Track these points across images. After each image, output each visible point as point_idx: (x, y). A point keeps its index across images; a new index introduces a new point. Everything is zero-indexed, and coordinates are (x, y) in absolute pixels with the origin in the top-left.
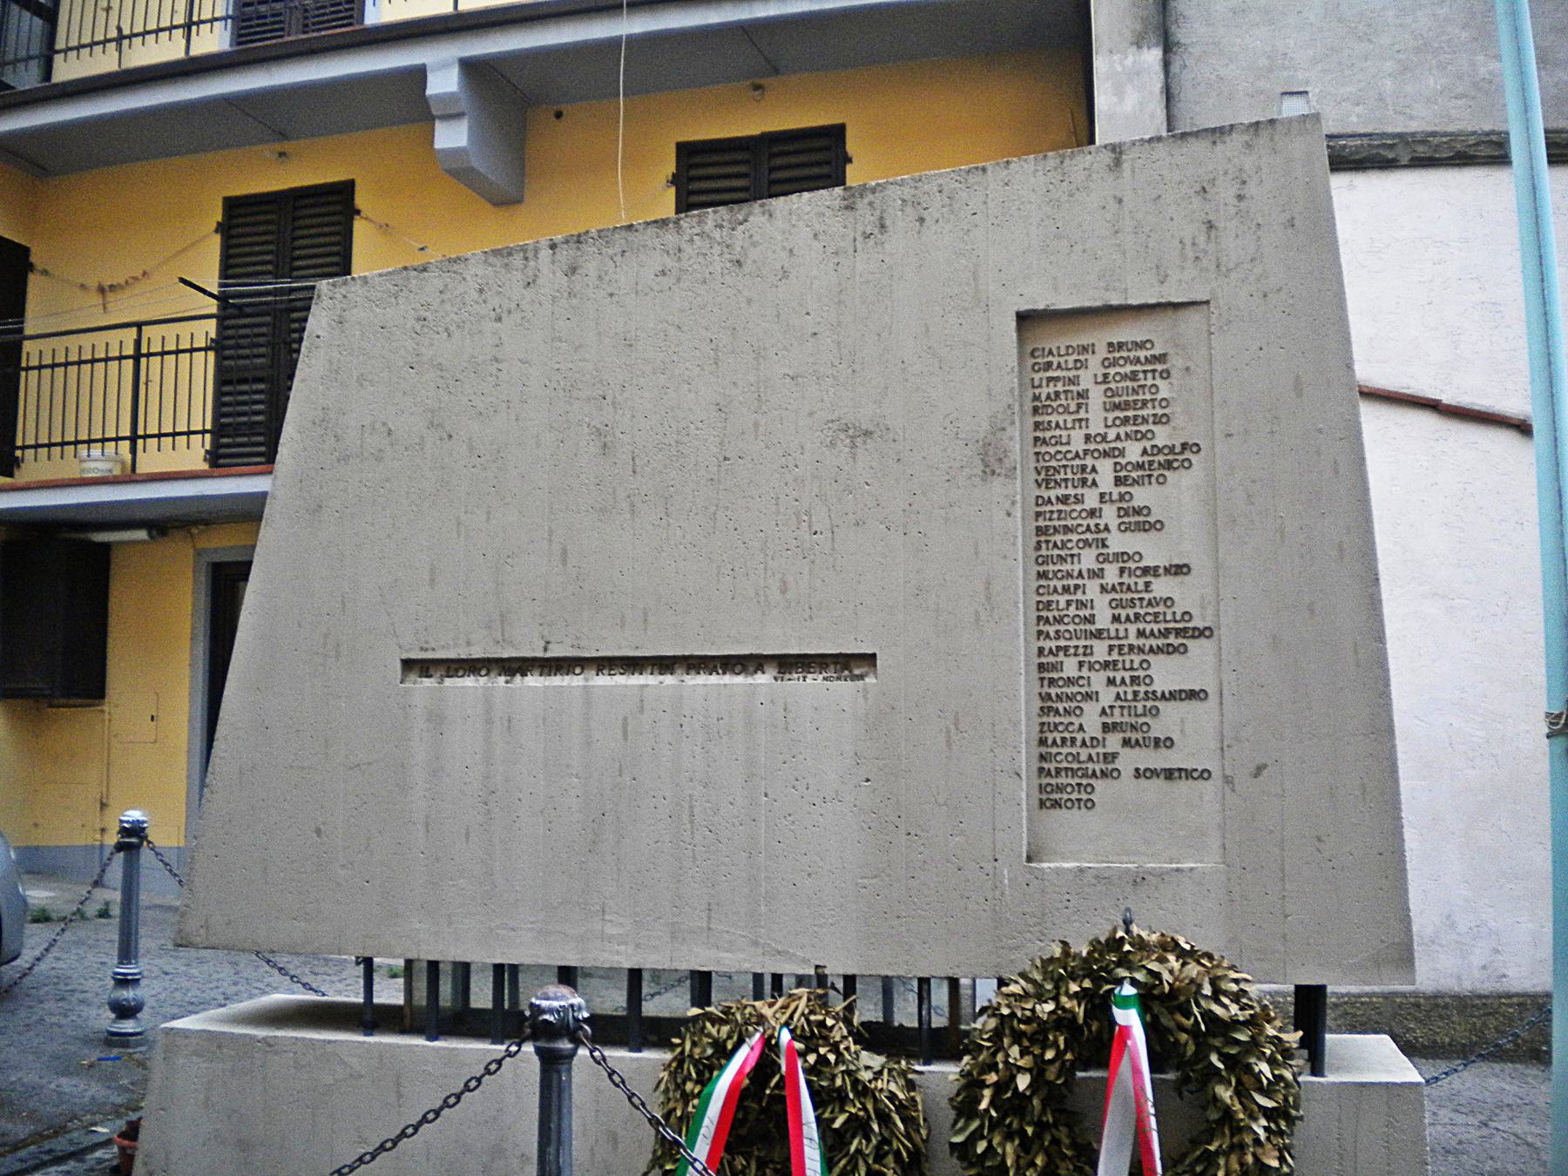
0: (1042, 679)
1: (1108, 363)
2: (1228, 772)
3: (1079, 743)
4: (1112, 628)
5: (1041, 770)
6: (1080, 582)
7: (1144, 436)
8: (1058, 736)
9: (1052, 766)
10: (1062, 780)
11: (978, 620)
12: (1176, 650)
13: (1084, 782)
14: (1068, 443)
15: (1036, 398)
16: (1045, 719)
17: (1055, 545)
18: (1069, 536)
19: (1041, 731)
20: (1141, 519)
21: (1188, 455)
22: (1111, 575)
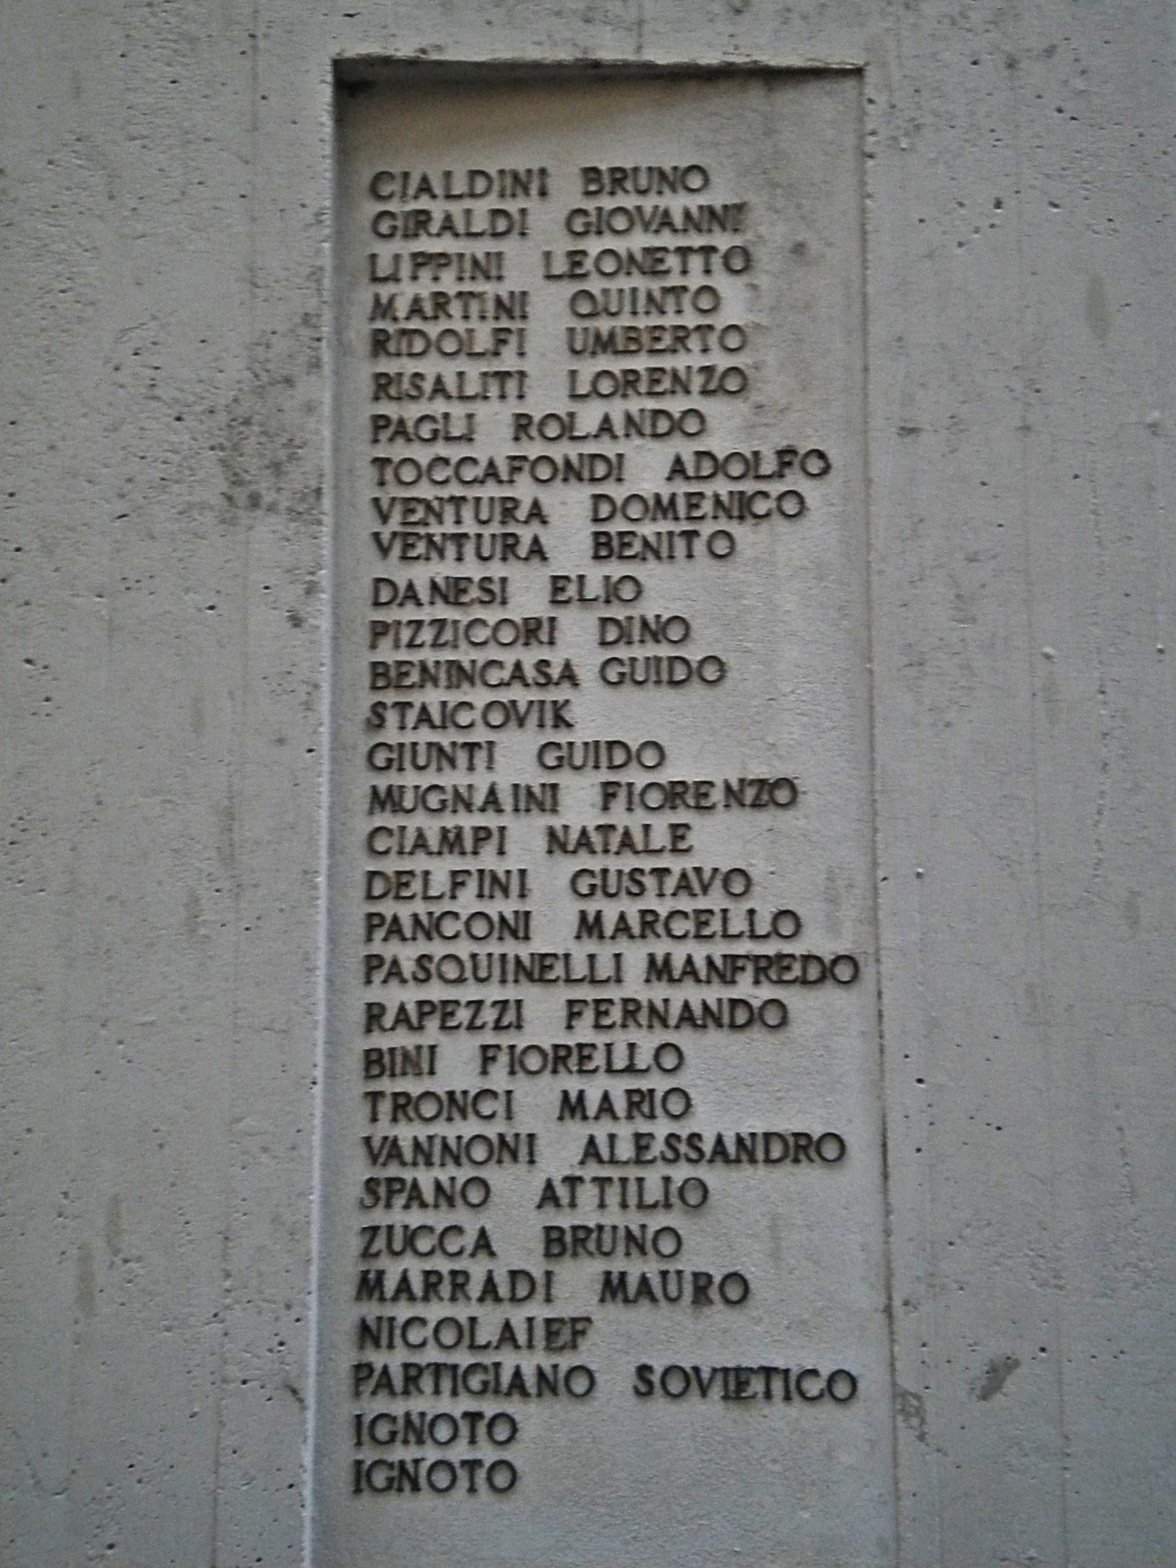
0: (375, 1097)
1: (581, 223)
2: (907, 1382)
3: (475, 1288)
4: (580, 952)
5: (362, 1371)
6: (490, 820)
7: (677, 426)
8: (415, 1268)
9: (394, 1360)
10: (423, 1404)
11: (193, 920)
12: (755, 1017)
13: (489, 1407)
14: (468, 438)
15: (383, 309)
16: (379, 1217)
17: (424, 716)
18: (466, 694)
19: (366, 1254)
20: (664, 651)
21: (794, 480)
22: (579, 803)
